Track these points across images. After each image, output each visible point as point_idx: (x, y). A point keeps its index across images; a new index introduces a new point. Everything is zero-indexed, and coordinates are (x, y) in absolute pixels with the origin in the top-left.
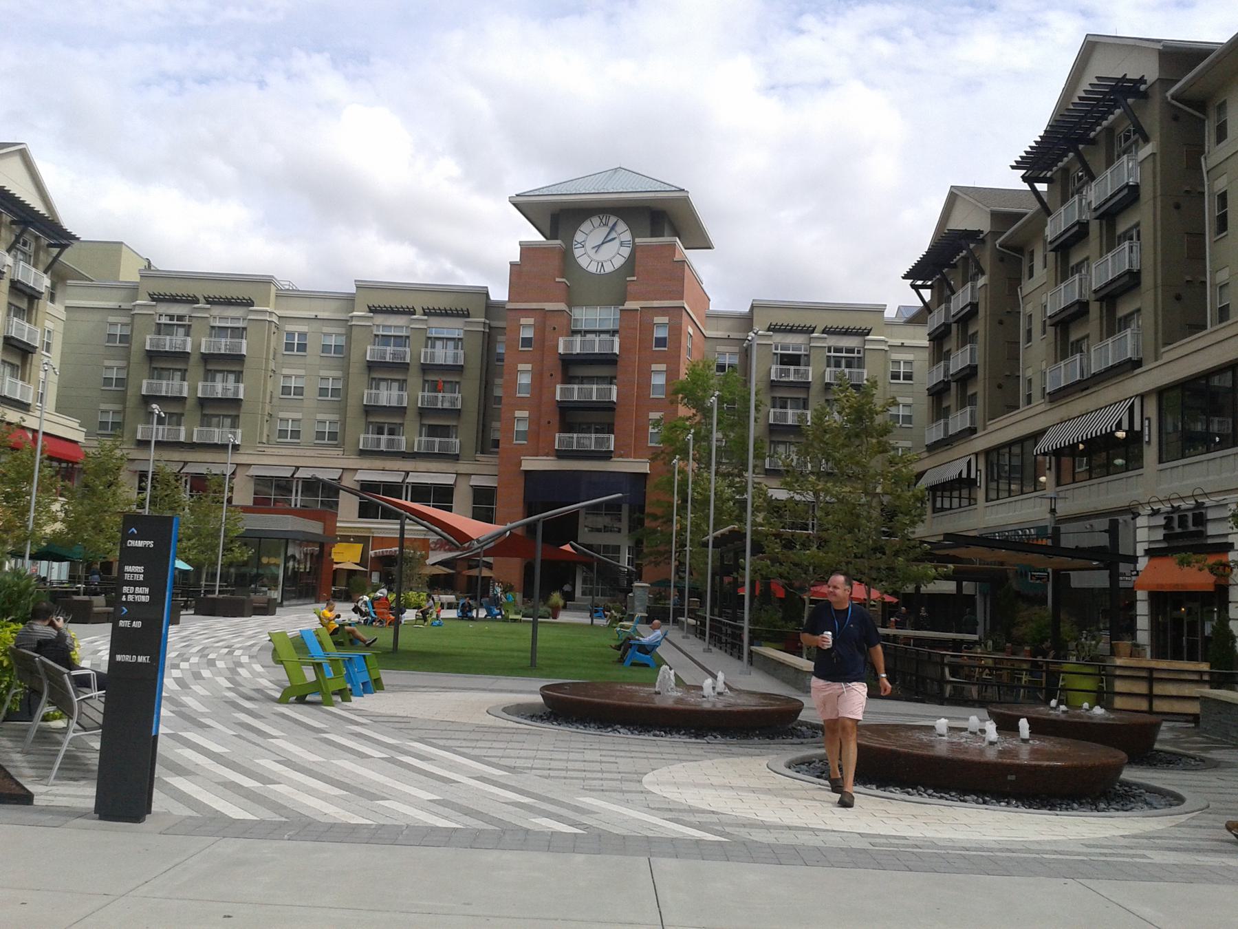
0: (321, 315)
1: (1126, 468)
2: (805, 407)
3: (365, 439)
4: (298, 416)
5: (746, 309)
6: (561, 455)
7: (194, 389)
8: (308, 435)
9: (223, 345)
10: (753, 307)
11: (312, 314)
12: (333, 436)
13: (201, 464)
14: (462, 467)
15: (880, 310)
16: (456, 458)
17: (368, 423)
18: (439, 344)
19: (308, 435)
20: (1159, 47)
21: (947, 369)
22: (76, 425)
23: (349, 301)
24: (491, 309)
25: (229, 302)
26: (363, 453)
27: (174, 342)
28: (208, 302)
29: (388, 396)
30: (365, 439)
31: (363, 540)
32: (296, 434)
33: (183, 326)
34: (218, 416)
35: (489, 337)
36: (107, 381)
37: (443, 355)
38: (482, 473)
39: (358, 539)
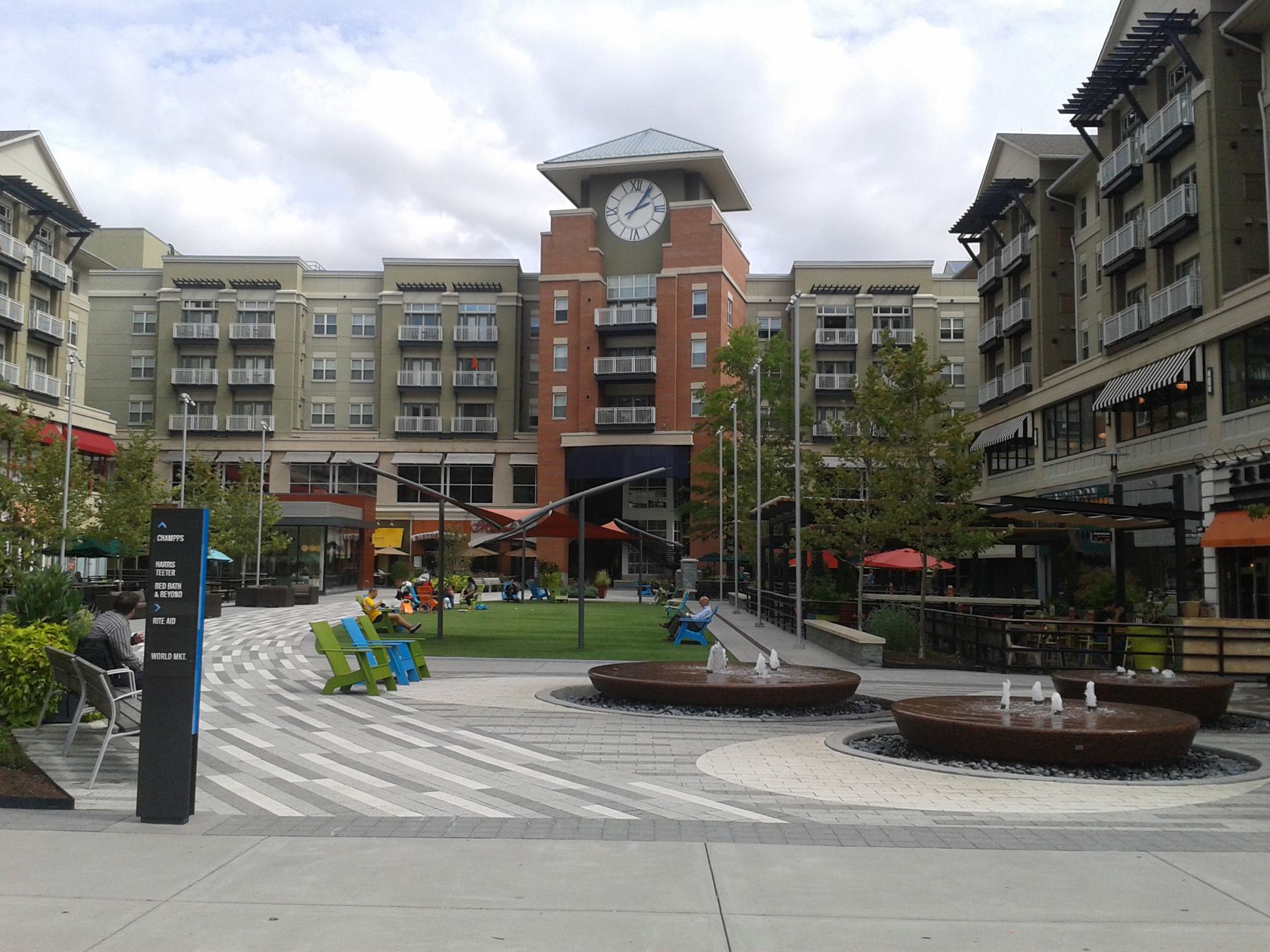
0: (350, 295)
4: (331, 400)
7: (224, 376)
8: (342, 419)
9: (251, 330)
10: (794, 269)
11: (340, 295)
12: (368, 419)
13: (235, 452)
14: (501, 446)
15: (926, 267)
16: (494, 437)
19: (342, 419)
22: (106, 418)
23: (377, 280)
24: (524, 282)
26: (399, 436)
28: (234, 287)
30: (401, 421)
32: (330, 418)
37: (476, 332)
39: (399, 524)
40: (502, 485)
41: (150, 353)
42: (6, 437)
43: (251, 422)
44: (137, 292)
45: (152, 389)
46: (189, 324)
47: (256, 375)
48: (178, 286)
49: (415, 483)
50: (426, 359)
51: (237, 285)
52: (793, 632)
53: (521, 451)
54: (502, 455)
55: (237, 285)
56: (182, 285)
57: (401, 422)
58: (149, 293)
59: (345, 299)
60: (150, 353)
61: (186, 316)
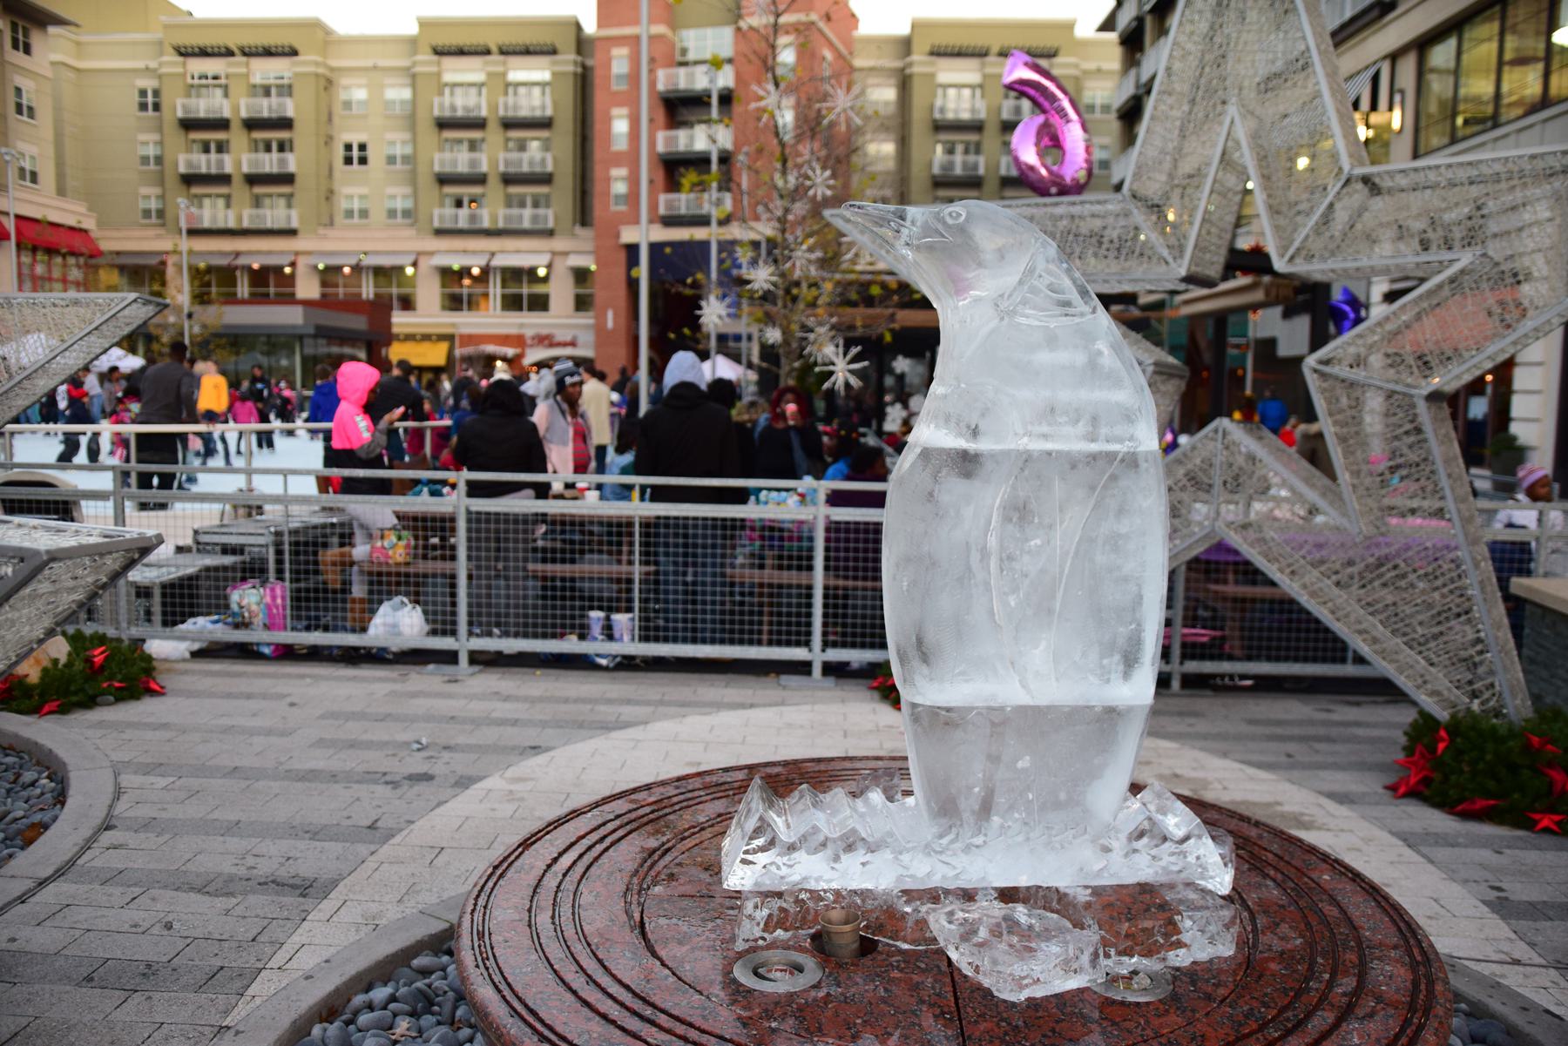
0: (382, 63)
1: (869, 284)
2: (978, 151)
3: (444, 214)
4: (364, 190)
5: (904, 30)
6: (670, 221)
7: (238, 164)
8: (378, 215)
9: (266, 108)
10: (913, 27)
11: (369, 63)
12: (407, 213)
13: (258, 253)
14: (558, 244)
15: (1068, 27)
16: (550, 233)
17: (443, 197)
18: (522, 90)
19: (378, 215)
20: (1297, 283)
21: (1138, 76)
22: (83, 210)
23: (412, 43)
24: (582, 44)
25: (268, 52)
26: (440, 232)
27: (208, 105)
28: (245, 54)
29: (460, 161)
30: (444, 214)
31: (449, 338)
32: (364, 213)
33: (220, 86)
34: (270, 196)
35: (584, 83)
36: (145, 160)
37: (532, 104)
38: (579, 251)
39: (442, 338)
40: (561, 292)
41: (156, 137)
42: (1219, 4)
43: (275, 214)
44: (141, 65)
45: (161, 181)
46: (261, 211)
47: (214, 218)
48: (181, 54)
49: (459, 290)
50: (218, 196)
51: (248, 53)
52: (1355, 652)
53: (579, 251)
54: (556, 257)
55: (248, 53)
56: (184, 53)
57: (441, 217)
58: (153, 65)
59: (375, 68)
60: (156, 137)
61: (191, 90)
